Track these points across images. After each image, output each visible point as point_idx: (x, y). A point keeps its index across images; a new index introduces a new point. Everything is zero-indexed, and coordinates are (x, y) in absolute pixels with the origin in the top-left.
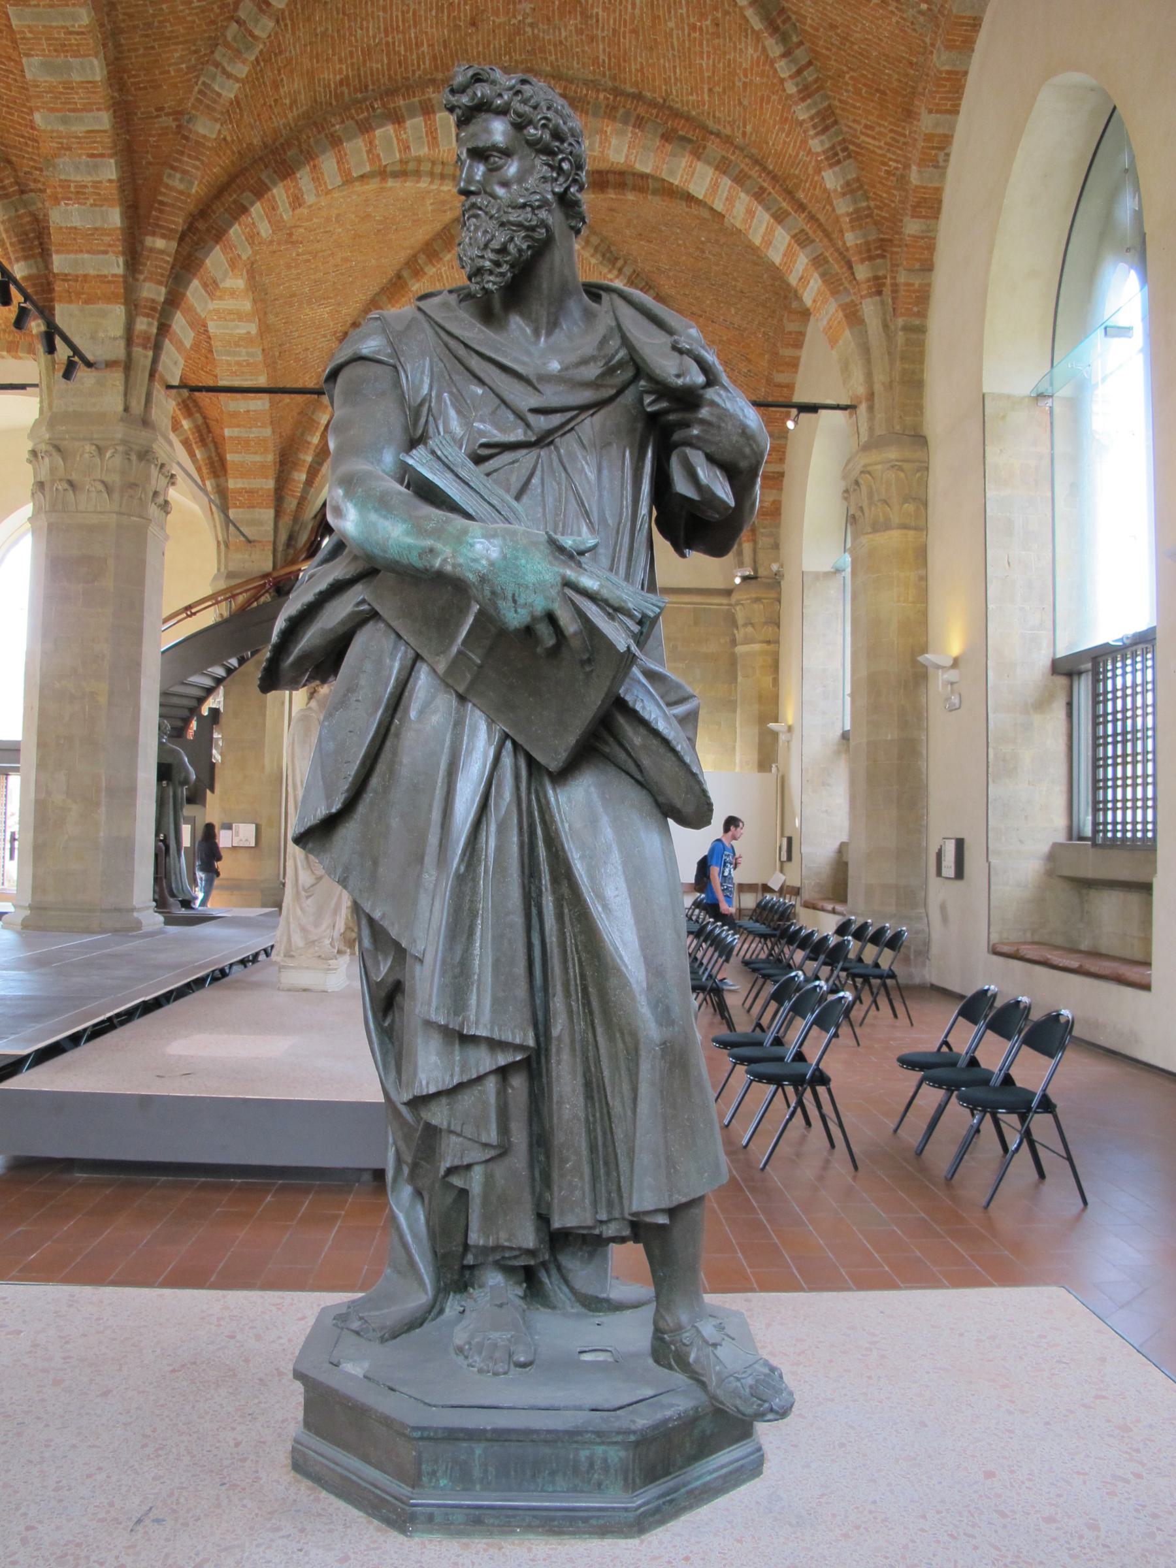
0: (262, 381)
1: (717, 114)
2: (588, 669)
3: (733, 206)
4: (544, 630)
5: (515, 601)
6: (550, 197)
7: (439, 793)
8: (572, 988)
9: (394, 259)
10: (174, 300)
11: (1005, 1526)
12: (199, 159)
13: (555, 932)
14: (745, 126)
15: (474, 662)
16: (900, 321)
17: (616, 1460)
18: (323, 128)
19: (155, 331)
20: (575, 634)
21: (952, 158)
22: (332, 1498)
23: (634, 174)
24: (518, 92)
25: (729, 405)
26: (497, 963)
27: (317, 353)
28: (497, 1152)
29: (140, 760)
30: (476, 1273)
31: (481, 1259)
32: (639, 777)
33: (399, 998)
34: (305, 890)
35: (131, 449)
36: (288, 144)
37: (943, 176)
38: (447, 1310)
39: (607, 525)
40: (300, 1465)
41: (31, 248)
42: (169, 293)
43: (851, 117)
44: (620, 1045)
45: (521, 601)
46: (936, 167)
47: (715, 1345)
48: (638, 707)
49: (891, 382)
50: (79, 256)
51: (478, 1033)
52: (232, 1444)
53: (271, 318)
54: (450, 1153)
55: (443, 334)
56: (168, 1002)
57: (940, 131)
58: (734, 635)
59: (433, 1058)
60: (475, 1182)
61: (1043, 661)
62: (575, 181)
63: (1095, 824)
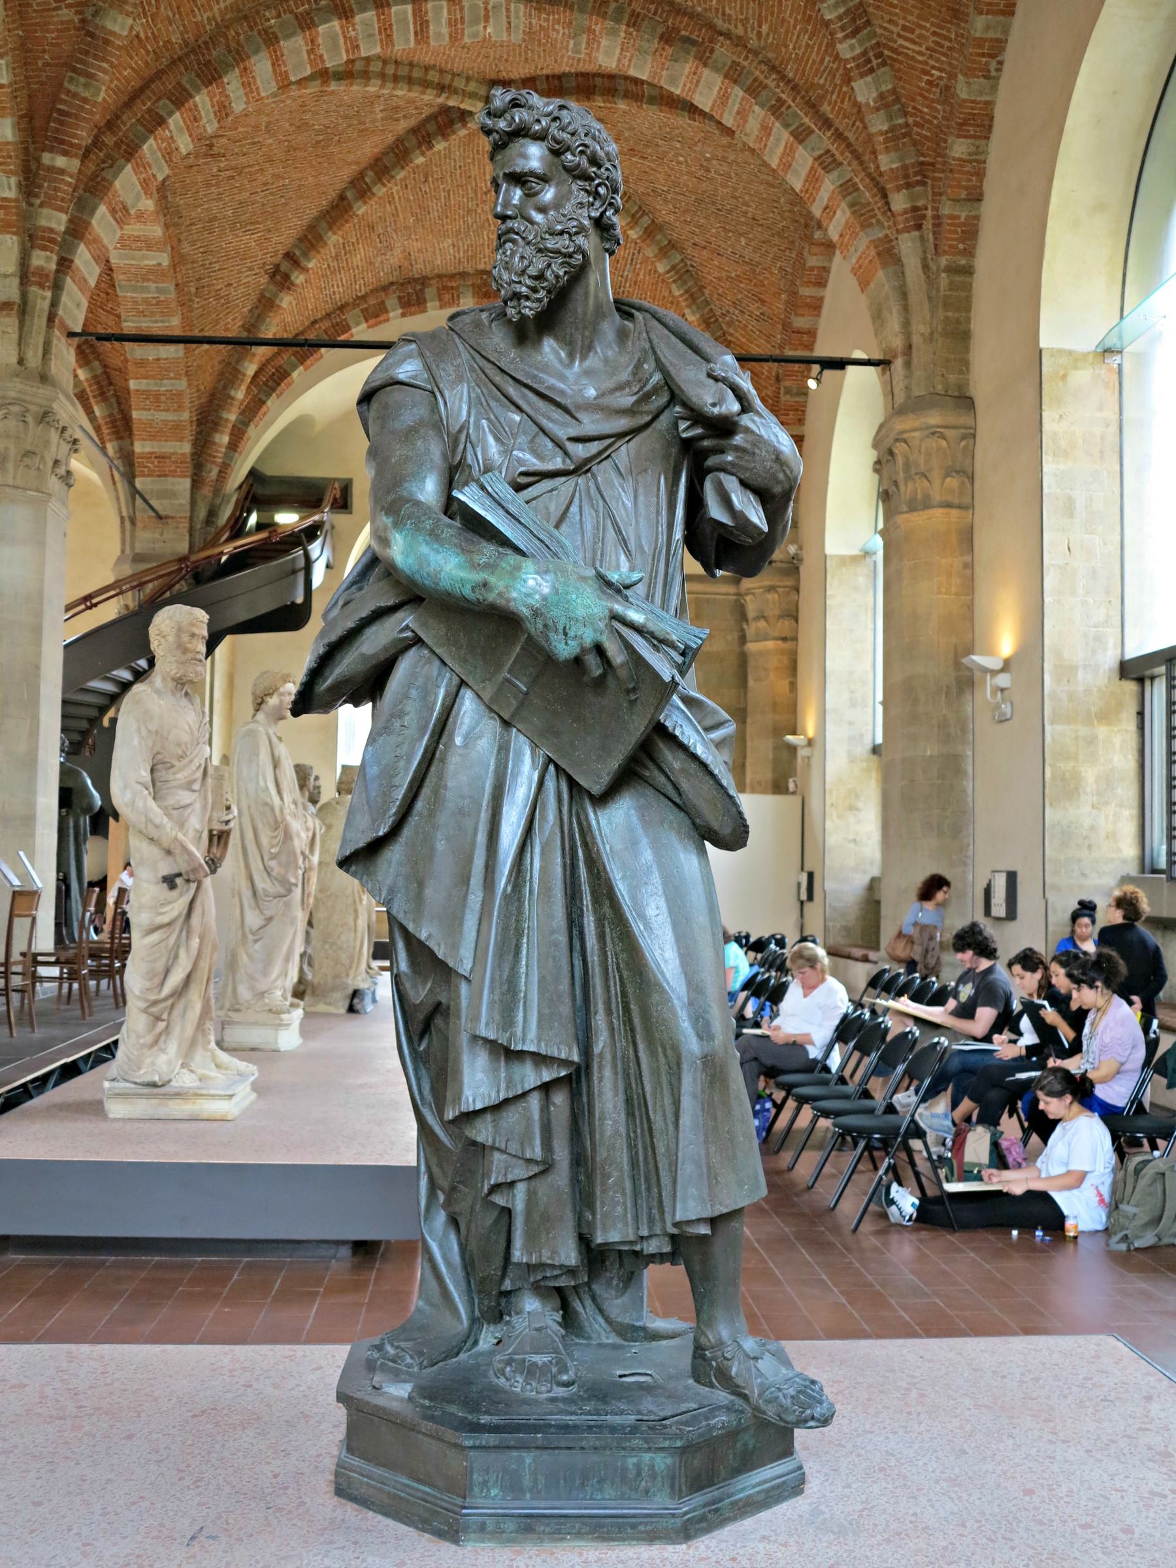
0: (174, 324)
1: (728, 11)
2: (633, 697)
3: (746, 121)
4: (592, 661)
5: (565, 634)
6: (586, 222)
8: (614, 1006)
9: (337, 178)
10: (77, 230)
11: (1042, 1532)
12: (107, 61)
13: (596, 952)
14: (760, 26)
15: (521, 691)
16: (944, 261)
17: (663, 1466)
18: (256, 23)
19: (53, 267)
20: (622, 665)
21: (1007, 67)
22: (380, 1517)
24: (555, 119)
25: (763, 432)
26: (542, 980)
27: (242, 289)
28: (541, 1168)
29: (40, 783)
30: (513, 1300)
31: (519, 1284)
32: (677, 800)
33: (438, 1021)
34: (253, 934)
35: (27, 410)
36: (213, 40)
37: (994, 89)
38: (481, 1342)
39: (643, 552)
40: (343, 1490)
42: (70, 221)
43: (887, 17)
44: (662, 1060)
45: (571, 633)
47: (756, 1358)
48: (677, 733)
49: (932, 334)
51: (525, 1048)
52: (270, 1475)
53: (186, 248)
54: (498, 1168)
55: (477, 356)
57: (991, 35)
58: (743, 630)
59: (480, 1076)
60: (519, 1200)
61: (1109, 659)
62: (611, 204)
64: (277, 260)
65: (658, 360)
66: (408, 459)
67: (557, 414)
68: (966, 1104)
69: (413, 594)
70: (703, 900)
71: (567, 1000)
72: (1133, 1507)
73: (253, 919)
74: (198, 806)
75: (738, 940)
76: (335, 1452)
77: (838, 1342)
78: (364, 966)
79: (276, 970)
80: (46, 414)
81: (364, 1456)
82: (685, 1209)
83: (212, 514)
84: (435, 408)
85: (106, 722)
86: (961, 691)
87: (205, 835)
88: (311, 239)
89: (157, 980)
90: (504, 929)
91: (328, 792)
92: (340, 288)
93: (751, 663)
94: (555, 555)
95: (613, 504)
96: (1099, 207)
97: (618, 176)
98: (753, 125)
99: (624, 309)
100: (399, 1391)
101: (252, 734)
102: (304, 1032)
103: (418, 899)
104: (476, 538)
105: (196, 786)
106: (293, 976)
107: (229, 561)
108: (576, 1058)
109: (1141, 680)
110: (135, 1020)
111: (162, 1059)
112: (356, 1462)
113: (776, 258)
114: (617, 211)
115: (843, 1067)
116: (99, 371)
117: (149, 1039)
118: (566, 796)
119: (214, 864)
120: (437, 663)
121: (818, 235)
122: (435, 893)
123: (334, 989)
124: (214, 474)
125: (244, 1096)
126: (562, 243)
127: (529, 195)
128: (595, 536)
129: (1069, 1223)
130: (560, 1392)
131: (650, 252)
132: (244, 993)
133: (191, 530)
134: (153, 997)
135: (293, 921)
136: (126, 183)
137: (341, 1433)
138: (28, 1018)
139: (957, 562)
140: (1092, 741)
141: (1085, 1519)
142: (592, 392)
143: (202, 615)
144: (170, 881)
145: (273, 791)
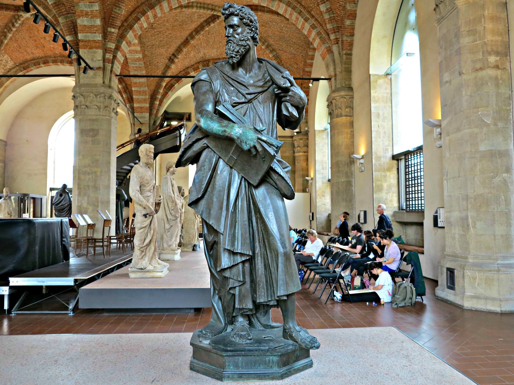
0: (144, 73)
4: (253, 150)
7: (226, 192)
10: (118, 48)
16: (344, 52)
19: (112, 58)
23: (260, 6)
24: (241, 10)
25: (296, 91)
29: (111, 193)
33: (215, 246)
37: (357, 6)
40: (192, 368)
41: (71, 32)
42: (116, 46)
45: (247, 143)
46: (355, 3)
50: (87, 34)
56: (99, 278)
59: (226, 259)
60: (237, 292)
61: (390, 155)
63: (406, 205)
64: (170, 56)
65: (269, 73)
66: (204, 100)
67: (243, 88)
68: (355, 271)
69: (207, 134)
70: (283, 210)
71: (248, 239)
72: (399, 369)
73: (167, 226)
74: (152, 196)
75: (294, 230)
76: (190, 359)
77: (321, 330)
78: (196, 238)
79: (174, 239)
80: (110, 96)
81: (197, 359)
82: (280, 293)
83: (155, 122)
84: (211, 87)
85: (128, 177)
86: (351, 164)
87: (154, 204)
88: (179, 50)
89: (142, 242)
90: (232, 221)
91: (186, 193)
92: (187, 63)
93: (296, 159)
94: (243, 123)
95: (258, 111)
96: (385, 37)
97: (258, 25)
98: (294, 17)
99: (260, 60)
100: (207, 342)
101: (166, 178)
102: (181, 256)
103: (209, 214)
104: (222, 119)
105: (152, 191)
106: (178, 241)
107: (160, 134)
108: (251, 254)
109: (398, 160)
110: (137, 252)
111: (144, 262)
112: (195, 361)
113: (301, 53)
114: (257, 34)
115: (322, 261)
116: (124, 85)
117: (141, 257)
118: (247, 186)
119: (157, 211)
120: (213, 152)
121: (311, 46)
122: (213, 212)
123: (189, 244)
124: (155, 112)
125: (166, 272)
126: (243, 43)
127: (234, 31)
128: (253, 119)
129: (382, 300)
130: (248, 341)
131: (268, 52)
132: (165, 245)
133: (149, 126)
134: (141, 246)
135: (178, 226)
136: (130, 35)
137: (191, 355)
138: (109, 253)
139: (349, 131)
140: (385, 176)
141: (386, 372)
142: (252, 82)
143: (152, 146)
144: (145, 216)
145: (172, 193)
